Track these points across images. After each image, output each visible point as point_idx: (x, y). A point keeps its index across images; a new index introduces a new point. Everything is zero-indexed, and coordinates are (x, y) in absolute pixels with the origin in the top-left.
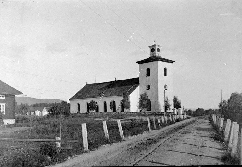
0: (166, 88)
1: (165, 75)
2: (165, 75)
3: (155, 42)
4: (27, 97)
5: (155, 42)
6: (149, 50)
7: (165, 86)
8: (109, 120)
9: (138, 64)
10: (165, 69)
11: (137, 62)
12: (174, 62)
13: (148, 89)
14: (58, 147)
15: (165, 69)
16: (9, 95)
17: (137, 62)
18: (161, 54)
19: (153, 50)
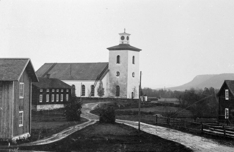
0: (134, 76)
1: (133, 63)
2: (133, 63)
3: (125, 30)
4: (95, 98)
5: (125, 30)
6: (120, 37)
7: (133, 73)
8: (138, 122)
9: (108, 50)
10: (133, 57)
11: (108, 49)
12: (141, 50)
13: (117, 76)
14: (30, 136)
15: (133, 57)
16: (102, 73)
17: (108, 49)
18: (132, 43)
19: (123, 38)
